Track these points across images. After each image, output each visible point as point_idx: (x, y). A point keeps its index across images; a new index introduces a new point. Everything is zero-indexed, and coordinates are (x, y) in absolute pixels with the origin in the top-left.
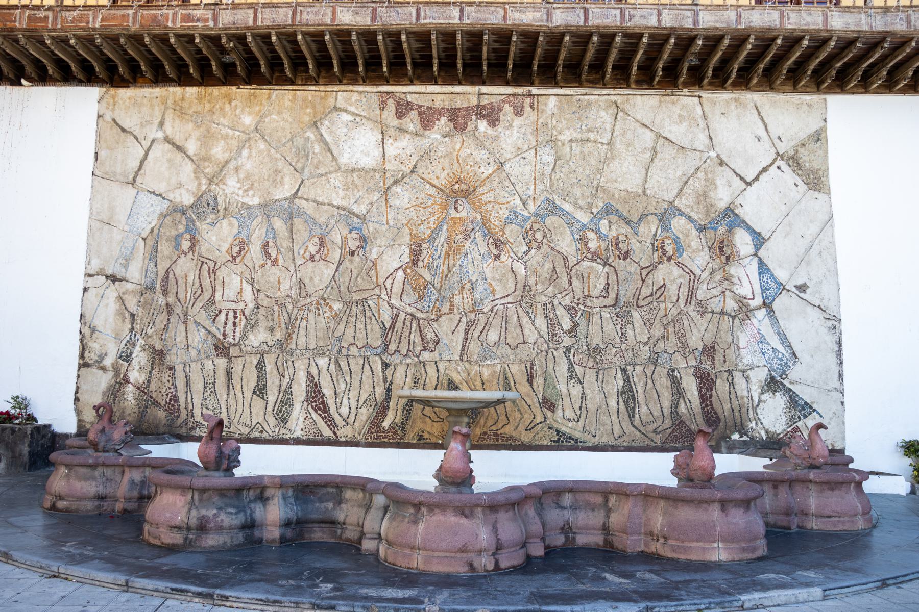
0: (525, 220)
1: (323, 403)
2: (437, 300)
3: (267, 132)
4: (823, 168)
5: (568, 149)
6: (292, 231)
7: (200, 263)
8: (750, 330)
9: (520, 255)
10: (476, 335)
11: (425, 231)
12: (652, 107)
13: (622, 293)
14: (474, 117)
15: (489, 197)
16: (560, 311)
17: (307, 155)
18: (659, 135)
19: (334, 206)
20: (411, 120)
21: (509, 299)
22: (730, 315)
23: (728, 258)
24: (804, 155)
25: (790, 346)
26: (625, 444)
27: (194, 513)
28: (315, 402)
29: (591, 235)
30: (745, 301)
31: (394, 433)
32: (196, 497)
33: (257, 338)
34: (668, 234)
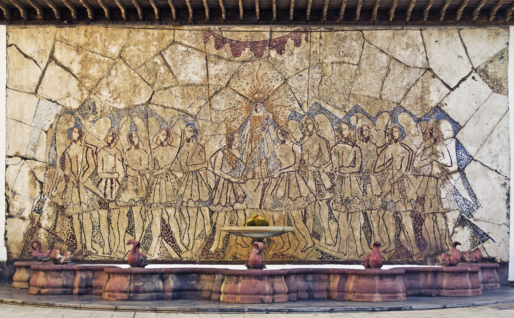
0: (302, 117)
1: (172, 237)
2: (244, 170)
5: (330, 69)
7: (86, 148)
8: (448, 187)
10: (270, 192)
11: (236, 125)
13: (364, 164)
14: (267, 48)
16: (324, 176)
17: (156, 75)
18: (392, 58)
19: (175, 109)
20: (226, 51)
21: (291, 169)
22: (435, 177)
24: (491, 70)
25: (475, 197)
27: (132, 285)
28: (167, 236)
29: (344, 126)
30: (445, 168)
31: (218, 255)
32: (132, 277)
33: (126, 197)
34: (396, 125)
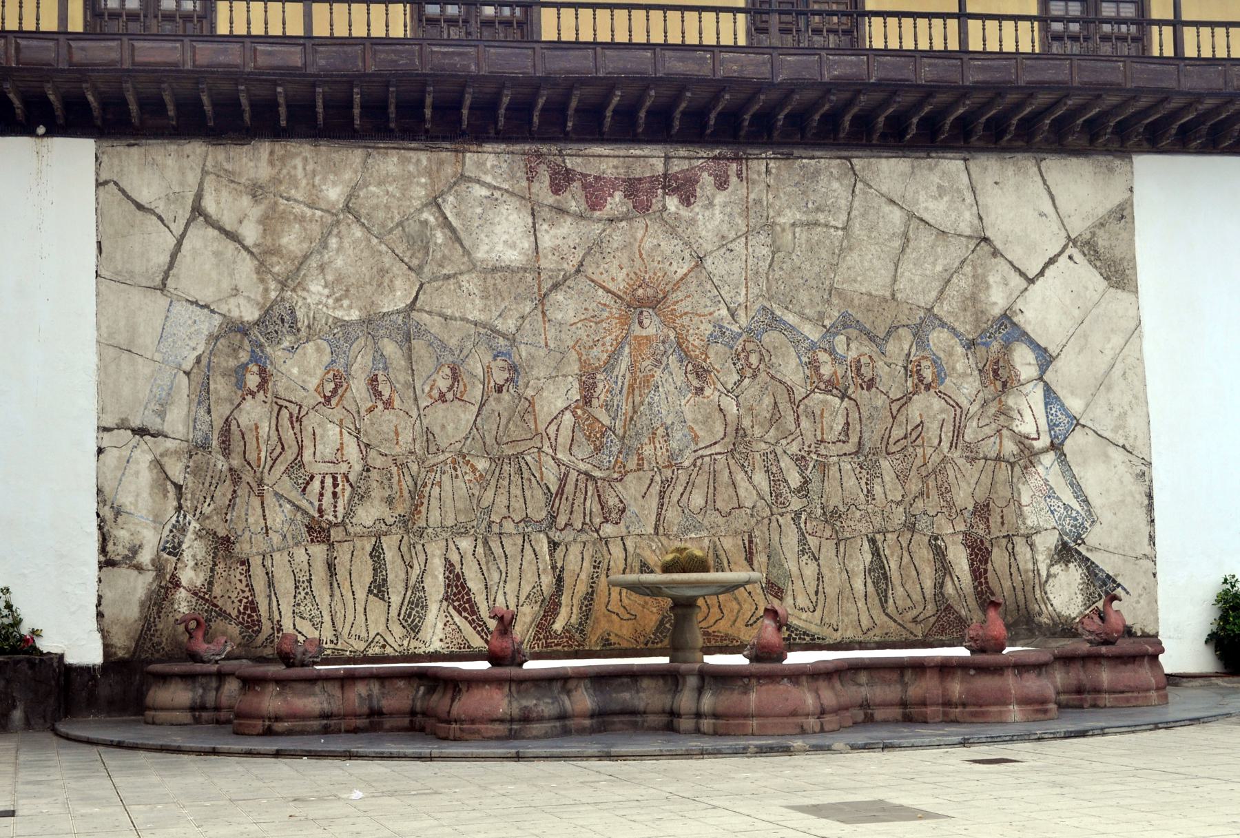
0: (735, 337)
1: (469, 601)
2: (620, 452)
3: (363, 211)
4: (1128, 257)
5: (790, 237)
6: (410, 358)
7: (276, 408)
8: (1034, 481)
9: (729, 387)
10: (675, 499)
11: (599, 355)
12: (902, 174)
13: (866, 435)
14: (660, 191)
15: (686, 306)
16: (786, 463)
17: (427, 248)
18: (911, 216)
19: (468, 321)
21: (717, 448)
23: (1004, 384)
24: (1102, 242)
25: (1086, 501)
26: (877, 639)
28: (458, 600)
29: (823, 357)
30: (1027, 442)
33: (367, 515)
